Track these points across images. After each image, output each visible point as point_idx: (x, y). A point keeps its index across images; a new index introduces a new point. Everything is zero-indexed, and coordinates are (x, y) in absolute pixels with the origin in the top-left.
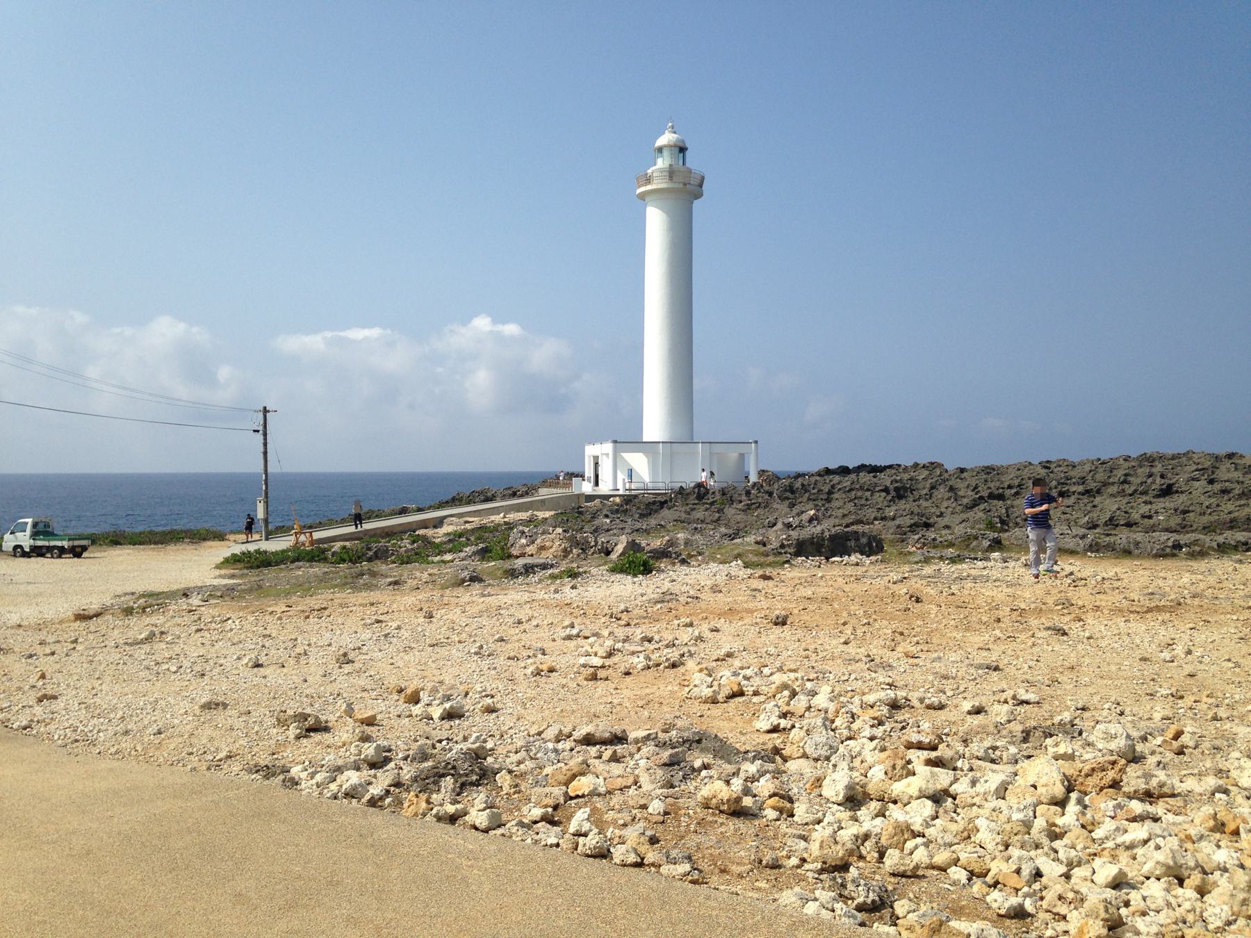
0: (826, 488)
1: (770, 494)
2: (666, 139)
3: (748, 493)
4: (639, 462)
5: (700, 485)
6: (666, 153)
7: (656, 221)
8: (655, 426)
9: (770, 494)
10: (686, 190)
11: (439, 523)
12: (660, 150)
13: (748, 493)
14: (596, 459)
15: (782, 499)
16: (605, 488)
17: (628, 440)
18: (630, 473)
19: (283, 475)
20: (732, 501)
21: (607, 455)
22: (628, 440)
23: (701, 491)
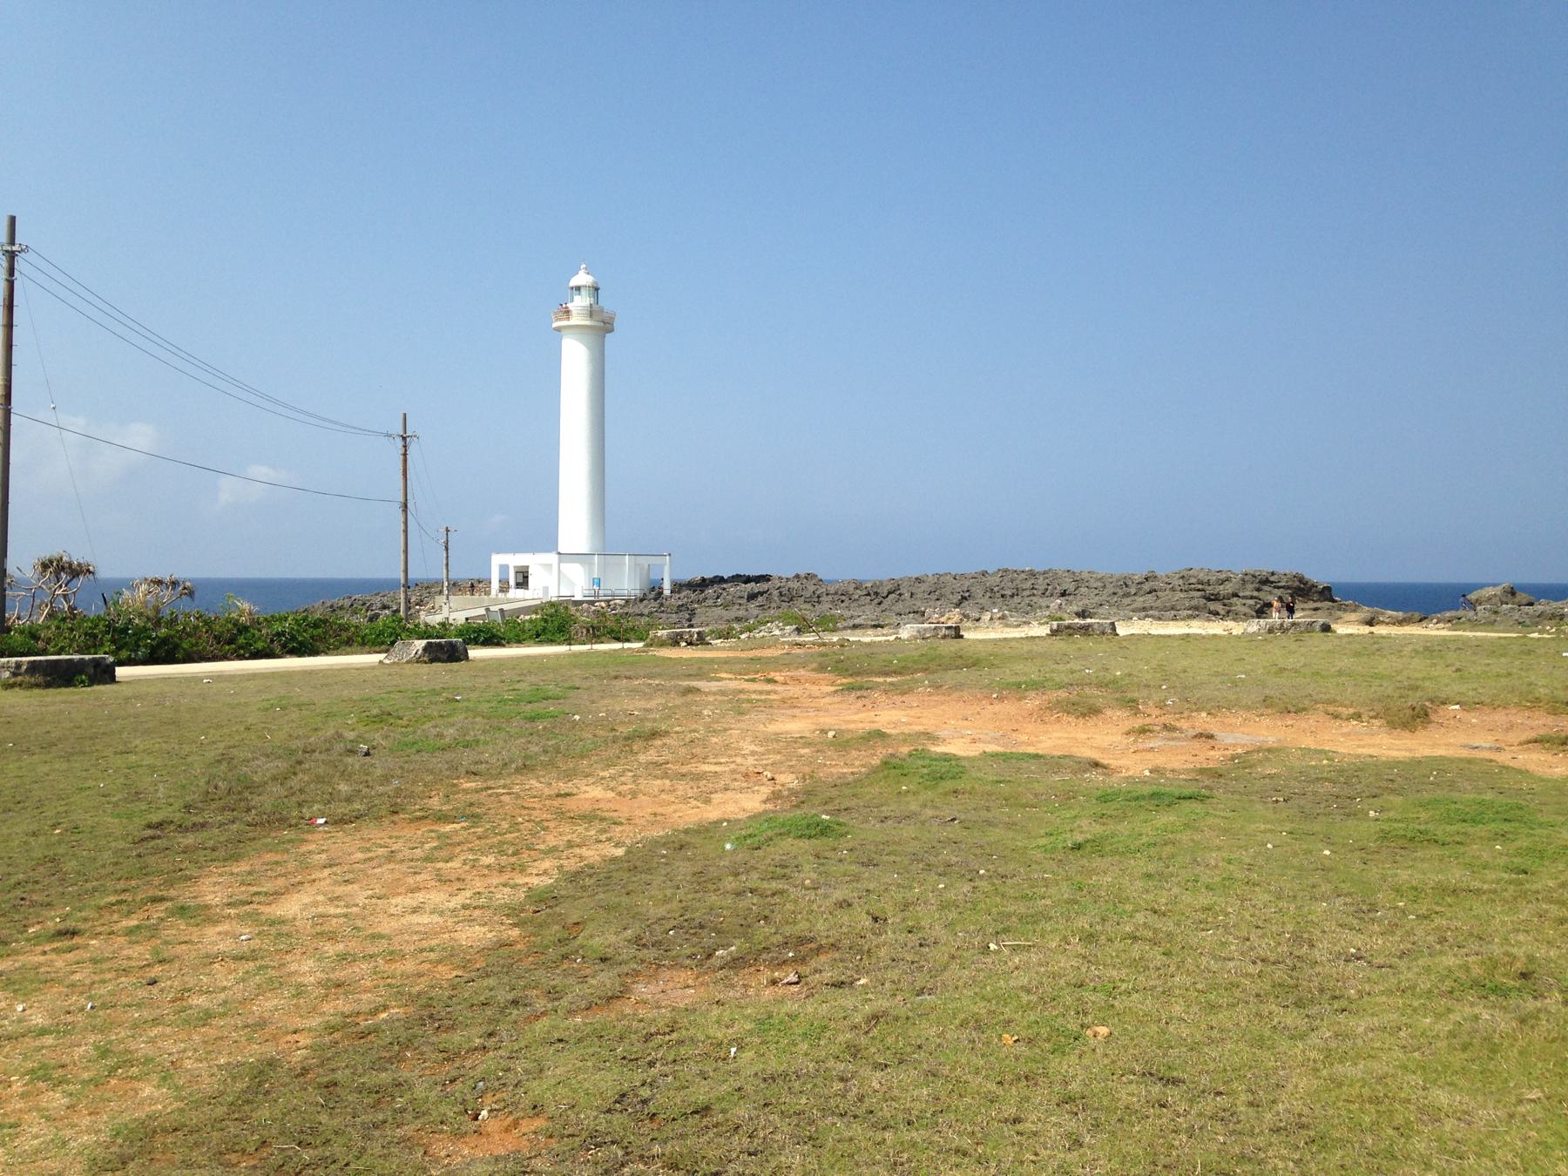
7: (575, 357)
12: (578, 288)
21: (548, 566)
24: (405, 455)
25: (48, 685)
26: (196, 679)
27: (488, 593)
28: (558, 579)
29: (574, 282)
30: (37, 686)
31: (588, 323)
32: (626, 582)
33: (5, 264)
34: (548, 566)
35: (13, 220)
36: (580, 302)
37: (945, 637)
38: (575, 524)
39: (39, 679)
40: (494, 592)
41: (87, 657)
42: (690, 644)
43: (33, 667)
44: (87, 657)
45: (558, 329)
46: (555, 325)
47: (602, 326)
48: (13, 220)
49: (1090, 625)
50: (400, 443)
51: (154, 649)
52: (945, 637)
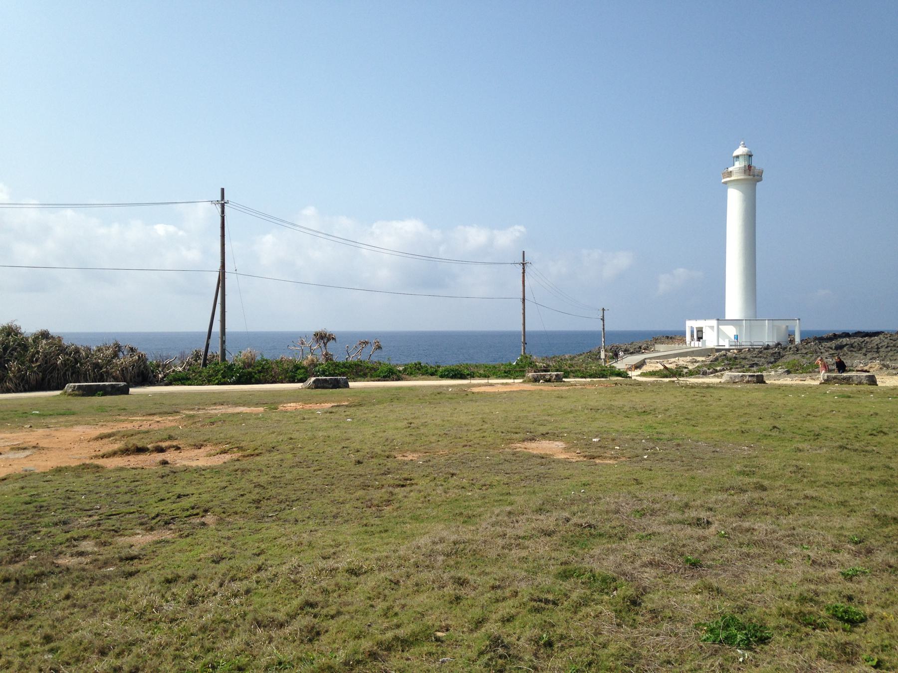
2: (741, 150)
6: (741, 159)
7: (735, 199)
12: (738, 157)
21: (712, 328)
24: (524, 273)
25: (83, 395)
26: (21, 399)
27: (684, 342)
28: (717, 336)
29: (736, 153)
30: (79, 395)
31: (742, 177)
32: (766, 336)
33: (220, 210)
34: (712, 328)
35: (223, 190)
36: (739, 165)
37: (748, 382)
38: (735, 304)
39: (81, 392)
40: (688, 343)
41: (107, 383)
42: (547, 381)
43: (80, 387)
44: (107, 383)
45: (726, 183)
46: (723, 181)
47: (752, 175)
48: (223, 190)
49: (850, 377)
50: (521, 267)
51: (240, 377)
52: (748, 382)
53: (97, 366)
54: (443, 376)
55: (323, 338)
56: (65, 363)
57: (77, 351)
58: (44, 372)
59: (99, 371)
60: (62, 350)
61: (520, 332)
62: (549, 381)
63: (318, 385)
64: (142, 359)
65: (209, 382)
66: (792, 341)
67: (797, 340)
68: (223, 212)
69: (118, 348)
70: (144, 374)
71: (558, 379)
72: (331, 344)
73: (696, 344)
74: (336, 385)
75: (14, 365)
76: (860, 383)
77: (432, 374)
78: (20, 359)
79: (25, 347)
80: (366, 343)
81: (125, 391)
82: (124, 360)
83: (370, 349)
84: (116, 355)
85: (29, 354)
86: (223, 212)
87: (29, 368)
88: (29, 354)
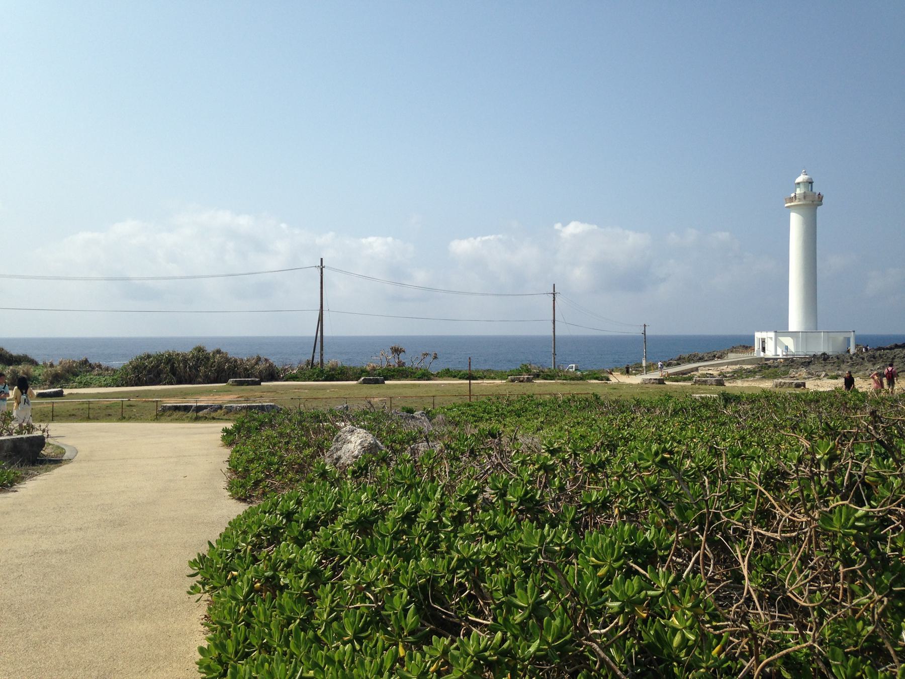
0: (891, 357)
1: (863, 359)
2: (801, 178)
3: (851, 358)
4: (789, 342)
5: (824, 354)
6: (801, 185)
7: (796, 221)
8: (795, 321)
9: (863, 359)
10: (813, 202)
11: (697, 369)
12: (799, 184)
13: (851, 358)
14: (763, 342)
15: (869, 361)
16: (770, 353)
17: (781, 329)
18: (787, 348)
19: (333, 338)
20: (843, 362)
21: (771, 338)
22: (781, 329)
23: (825, 357)
28: (773, 346)
32: (820, 347)
38: (795, 321)
53: (246, 369)
54: (460, 378)
55: (397, 351)
56: (229, 368)
57: (236, 361)
58: (218, 372)
59: (247, 373)
60: (227, 360)
61: (788, 328)
62: (522, 381)
63: (365, 382)
64: (271, 365)
65: (309, 380)
66: (848, 351)
67: (853, 350)
68: (322, 273)
69: (259, 359)
70: (272, 375)
71: (529, 380)
72: (402, 355)
73: (762, 354)
74: (376, 382)
75: (202, 369)
76: (711, 384)
77: (455, 377)
78: (205, 365)
79: (208, 359)
80: (427, 354)
81: (258, 383)
82: (262, 366)
83: (429, 359)
84: (257, 363)
85: (210, 363)
86: (322, 273)
87: (210, 370)
88: (210, 363)
